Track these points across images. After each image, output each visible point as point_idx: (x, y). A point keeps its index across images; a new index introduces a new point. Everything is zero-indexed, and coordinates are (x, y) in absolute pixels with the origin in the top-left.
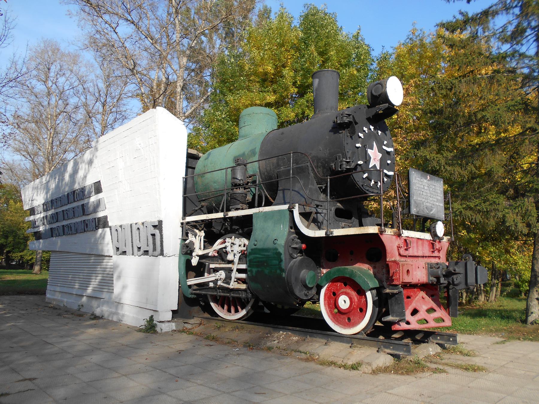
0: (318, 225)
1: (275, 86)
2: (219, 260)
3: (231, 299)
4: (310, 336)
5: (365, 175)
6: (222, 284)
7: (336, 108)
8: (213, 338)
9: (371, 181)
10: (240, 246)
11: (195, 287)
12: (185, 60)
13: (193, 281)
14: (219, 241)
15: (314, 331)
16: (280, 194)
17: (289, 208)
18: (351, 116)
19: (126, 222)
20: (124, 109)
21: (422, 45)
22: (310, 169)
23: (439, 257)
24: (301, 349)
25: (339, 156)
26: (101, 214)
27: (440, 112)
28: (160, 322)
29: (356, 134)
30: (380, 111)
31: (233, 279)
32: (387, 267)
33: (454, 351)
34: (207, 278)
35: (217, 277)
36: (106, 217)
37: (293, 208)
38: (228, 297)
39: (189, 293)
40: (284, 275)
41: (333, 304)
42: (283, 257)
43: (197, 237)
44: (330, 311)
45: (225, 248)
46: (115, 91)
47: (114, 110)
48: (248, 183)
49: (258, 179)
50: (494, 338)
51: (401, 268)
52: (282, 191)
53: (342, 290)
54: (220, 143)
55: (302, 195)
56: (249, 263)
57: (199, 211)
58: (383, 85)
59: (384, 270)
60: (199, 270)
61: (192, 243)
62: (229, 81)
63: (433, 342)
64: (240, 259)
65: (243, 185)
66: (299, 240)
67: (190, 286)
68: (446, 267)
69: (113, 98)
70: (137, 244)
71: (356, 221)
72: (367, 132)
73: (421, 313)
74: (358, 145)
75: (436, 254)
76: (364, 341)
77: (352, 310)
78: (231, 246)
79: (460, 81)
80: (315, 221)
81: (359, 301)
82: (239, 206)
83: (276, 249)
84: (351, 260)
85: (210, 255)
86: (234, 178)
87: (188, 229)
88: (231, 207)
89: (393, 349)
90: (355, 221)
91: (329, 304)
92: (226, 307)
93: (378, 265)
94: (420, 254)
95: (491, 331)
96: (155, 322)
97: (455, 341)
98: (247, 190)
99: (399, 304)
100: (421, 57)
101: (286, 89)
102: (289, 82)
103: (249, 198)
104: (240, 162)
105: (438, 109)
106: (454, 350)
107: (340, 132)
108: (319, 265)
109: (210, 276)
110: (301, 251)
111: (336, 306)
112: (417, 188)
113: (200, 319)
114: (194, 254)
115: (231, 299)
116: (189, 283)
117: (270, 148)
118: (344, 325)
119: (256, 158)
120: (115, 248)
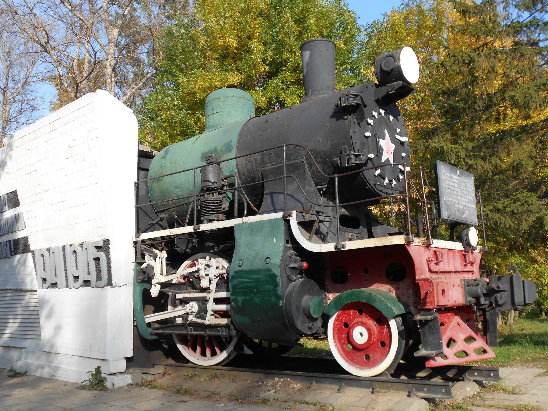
0: (321, 237)
1: (239, 63)
2: (189, 288)
3: (207, 339)
4: (316, 382)
5: (378, 172)
6: (194, 319)
7: (331, 87)
8: (186, 392)
9: (384, 179)
10: (217, 268)
11: (156, 326)
12: (116, 32)
13: (153, 318)
14: (187, 263)
15: (321, 375)
16: (267, 199)
17: (284, 216)
18: (359, 97)
19: (56, 243)
20: (32, 97)
21: (421, 12)
22: (306, 165)
23: (472, 272)
24: (307, 399)
25: (345, 149)
26: (20, 235)
27: (455, 92)
28: (111, 374)
29: (365, 121)
30: (391, 89)
31: (210, 312)
32: (416, 288)
33: (496, 389)
34: (171, 312)
35: (187, 311)
36: (26, 239)
37: (290, 216)
38: (202, 337)
39: (147, 334)
40: (281, 303)
41: (345, 338)
42: (279, 280)
43: (157, 259)
44: (341, 347)
45: (198, 271)
46: (19, 73)
47: (18, 98)
48: (223, 186)
49: (237, 182)
50: (532, 369)
51: (435, 287)
52: (269, 196)
53: (357, 320)
54: (173, 139)
55: (297, 200)
56: (233, 291)
57: (156, 225)
58: (395, 58)
59: (410, 291)
60: (159, 304)
61: (151, 267)
62: (176, 59)
63: (470, 380)
64: (217, 285)
65: (217, 189)
66: (298, 258)
67: (149, 325)
68: (486, 284)
69: (16, 82)
70: (72, 271)
71: (365, 231)
72: (377, 117)
73: (457, 344)
74: (368, 134)
75: (469, 268)
76: (389, 384)
77: (372, 344)
78: (205, 269)
79: (479, 54)
80: (318, 232)
81: (380, 332)
82: (213, 217)
83: (270, 270)
84: (366, 280)
85: (174, 282)
86: (205, 181)
87: (142, 250)
88: (202, 219)
89: (428, 392)
90: (363, 230)
91: (340, 339)
92: (198, 349)
93: (402, 285)
94: (452, 269)
95: (527, 361)
96: (103, 375)
97: (497, 377)
98: (223, 196)
99: (434, 333)
100: (420, 27)
101: (255, 67)
102: (257, 57)
103: (226, 205)
104: (211, 160)
105: (452, 89)
106: (496, 388)
107: (345, 117)
108: (325, 289)
109: (176, 309)
110: (301, 272)
111: (349, 340)
112: (447, 186)
113: (163, 367)
114: (154, 282)
115: (207, 339)
116: (148, 320)
117: (249, 141)
118: (362, 365)
119: (233, 154)
120: (41, 280)
